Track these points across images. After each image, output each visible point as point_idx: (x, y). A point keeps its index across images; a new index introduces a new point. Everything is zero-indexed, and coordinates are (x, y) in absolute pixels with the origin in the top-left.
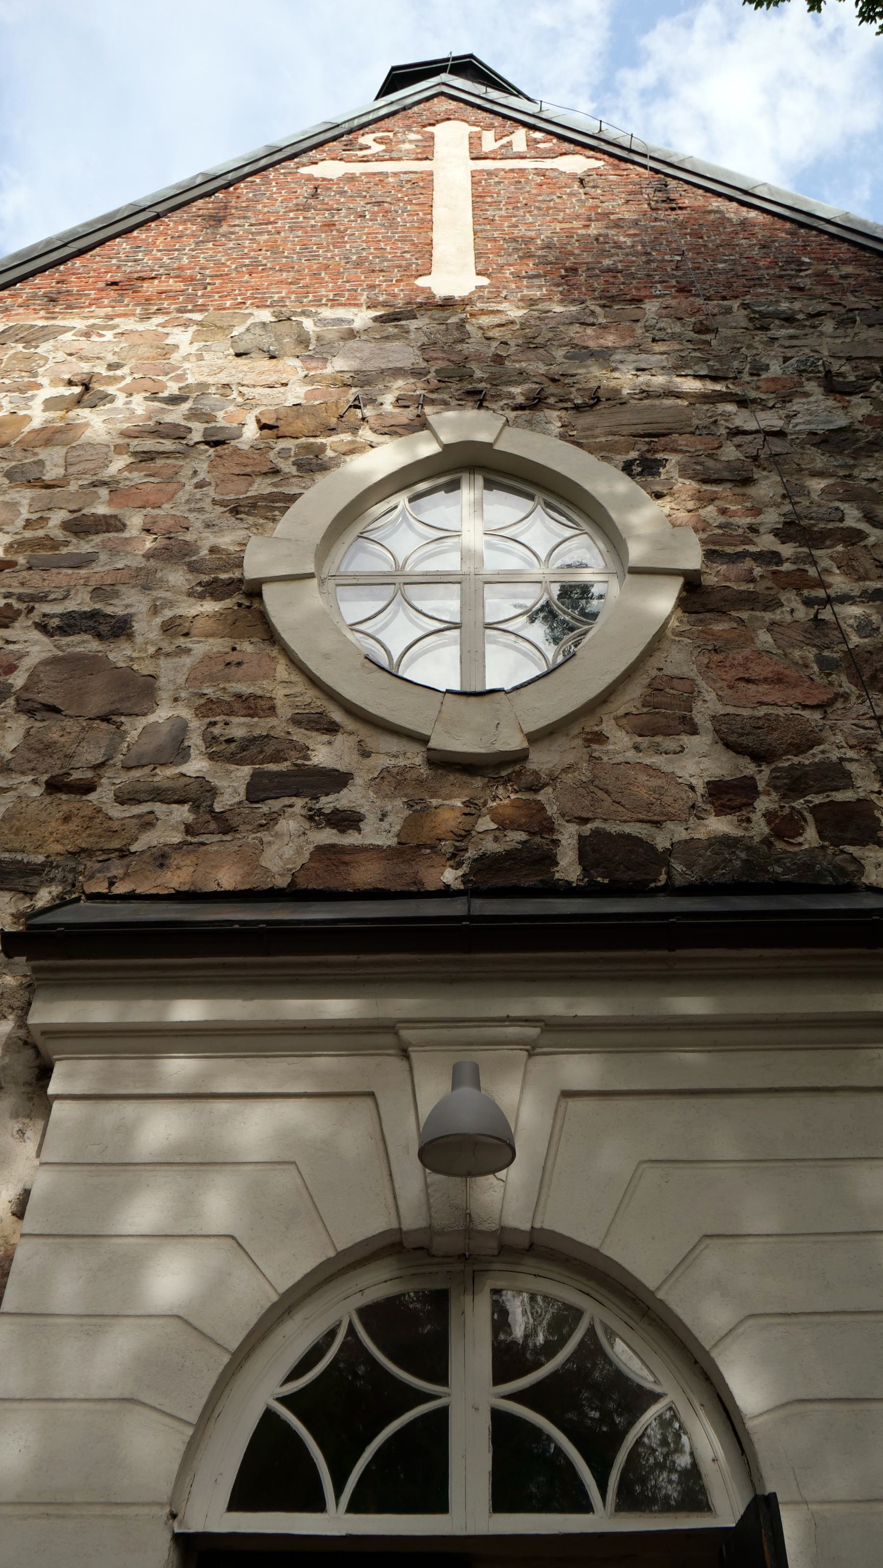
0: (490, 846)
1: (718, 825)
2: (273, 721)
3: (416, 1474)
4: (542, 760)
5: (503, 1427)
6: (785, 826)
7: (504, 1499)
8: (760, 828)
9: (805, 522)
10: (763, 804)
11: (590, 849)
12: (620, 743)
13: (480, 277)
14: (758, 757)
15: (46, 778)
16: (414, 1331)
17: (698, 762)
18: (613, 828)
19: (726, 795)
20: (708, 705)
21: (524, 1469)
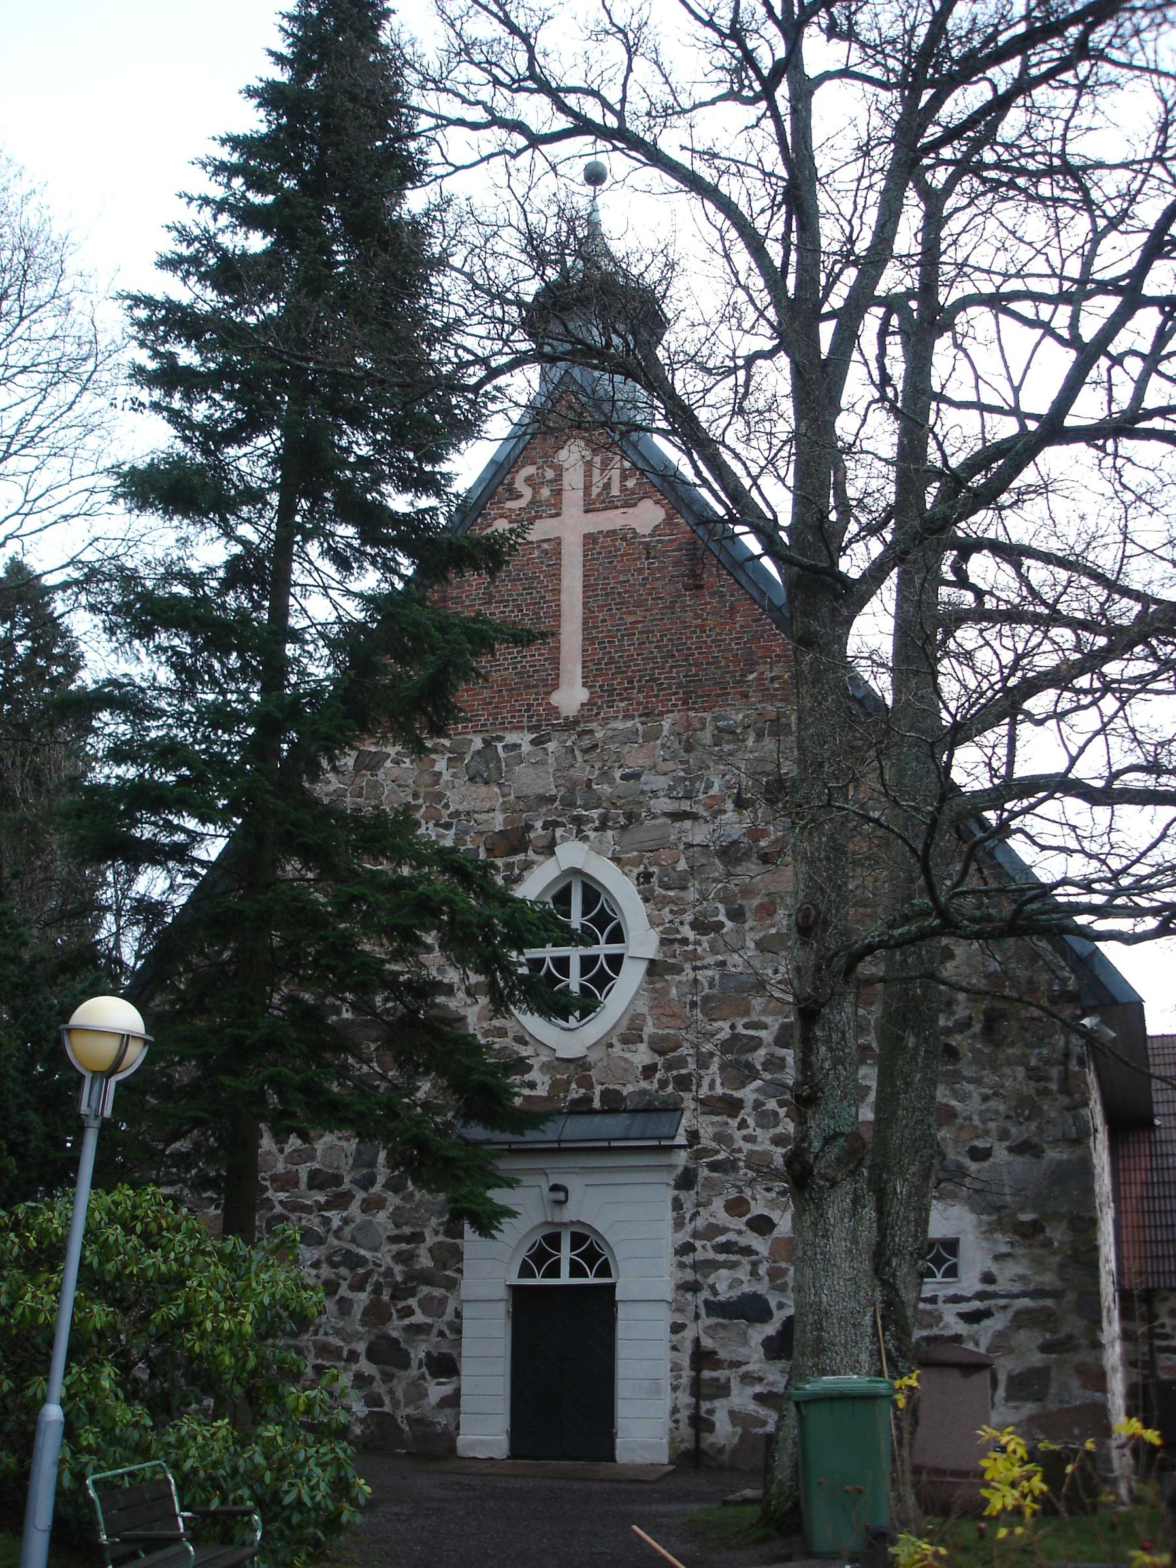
0: (576, 1096)
1: (644, 1085)
2: (507, 1040)
3: (554, 1271)
4: (593, 1057)
5: (572, 1261)
6: (663, 1084)
7: (573, 1274)
8: (656, 1085)
9: (176, 569)
10: (658, 1075)
11: (605, 1095)
12: (617, 1049)
13: (590, 515)
14: (661, 1053)
15: (469, 1020)
16: (553, 1240)
17: (642, 1055)
18: (611, 1087)
19: (649, 1071)
20: (649, 1029)
21: (576, 1270)
